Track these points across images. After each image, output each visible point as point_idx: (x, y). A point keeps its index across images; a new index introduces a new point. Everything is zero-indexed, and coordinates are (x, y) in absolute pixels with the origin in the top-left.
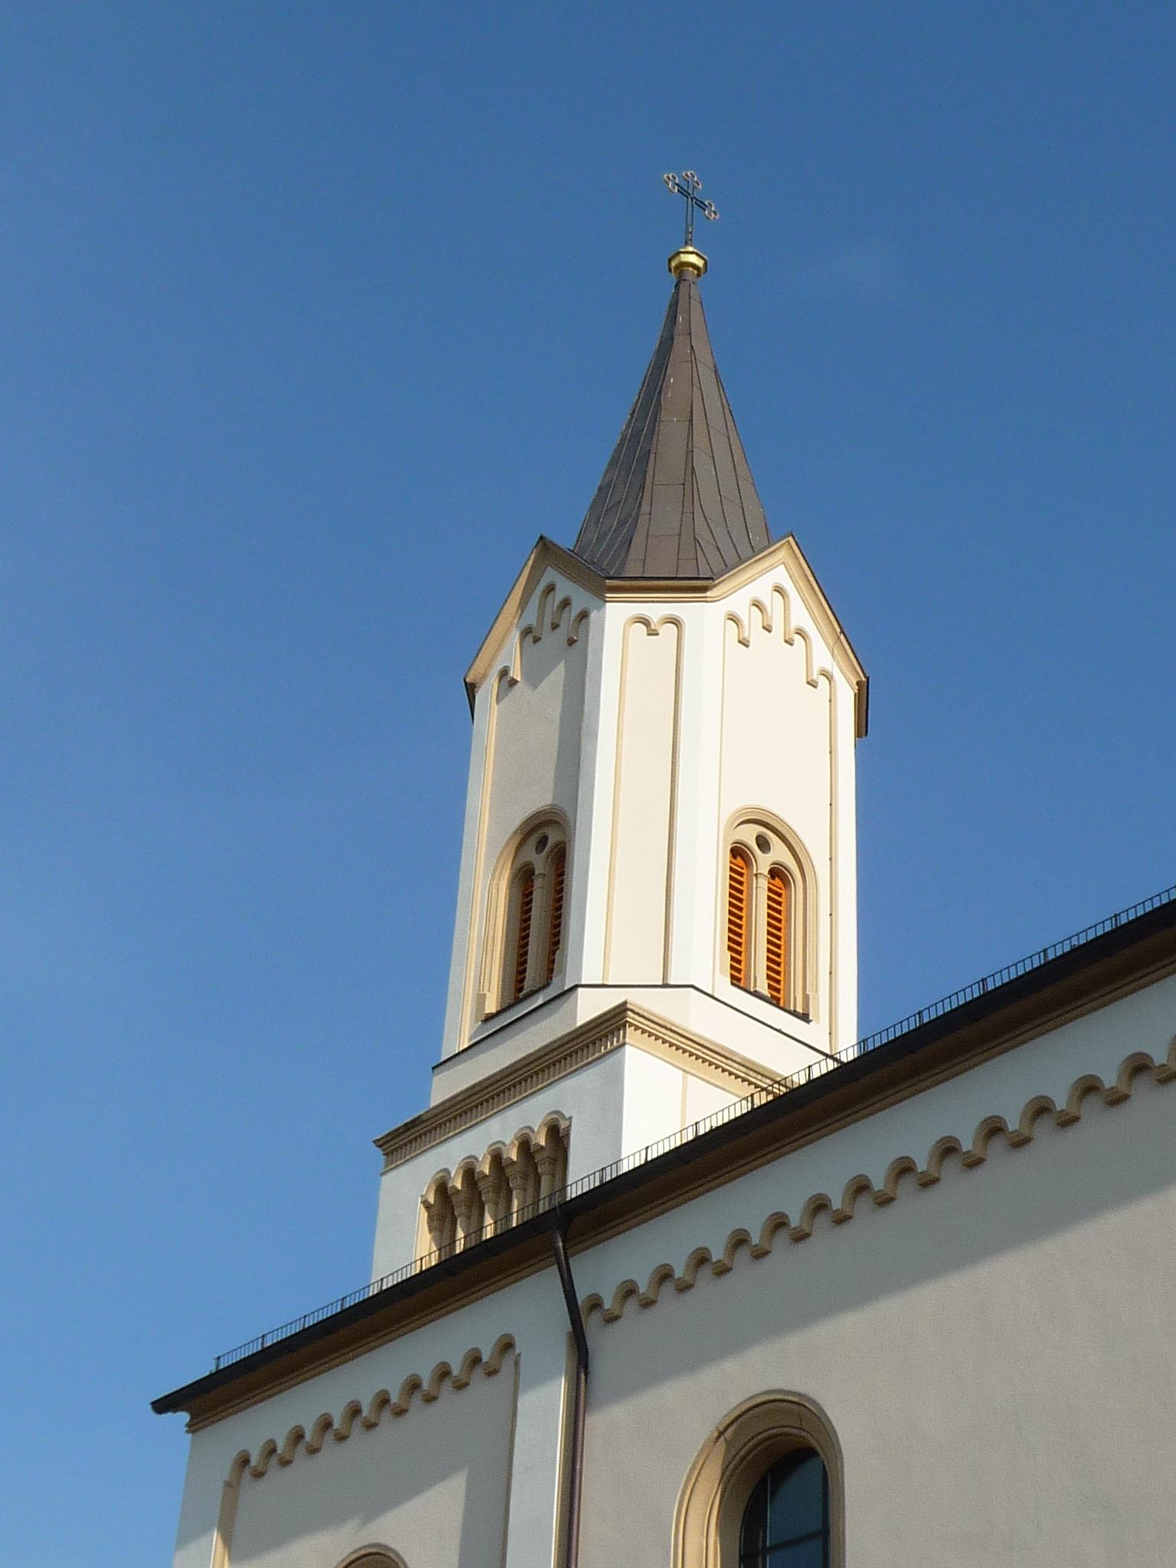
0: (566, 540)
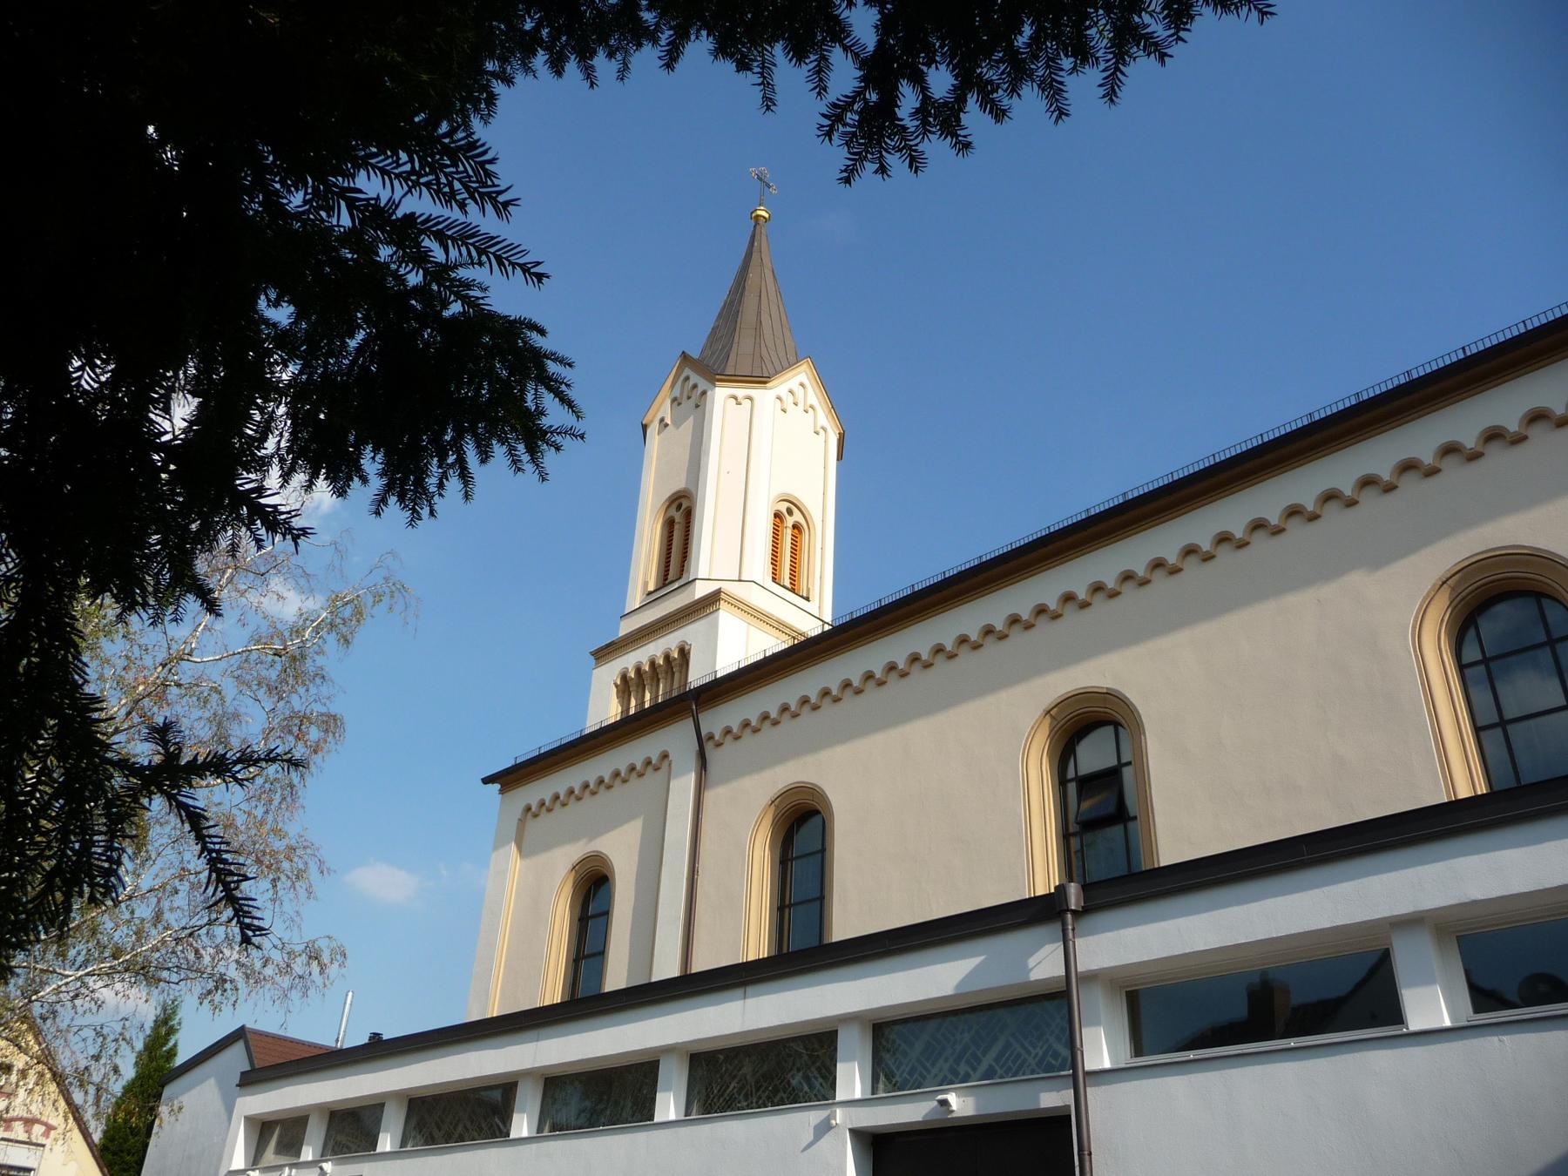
0: (695, 354)
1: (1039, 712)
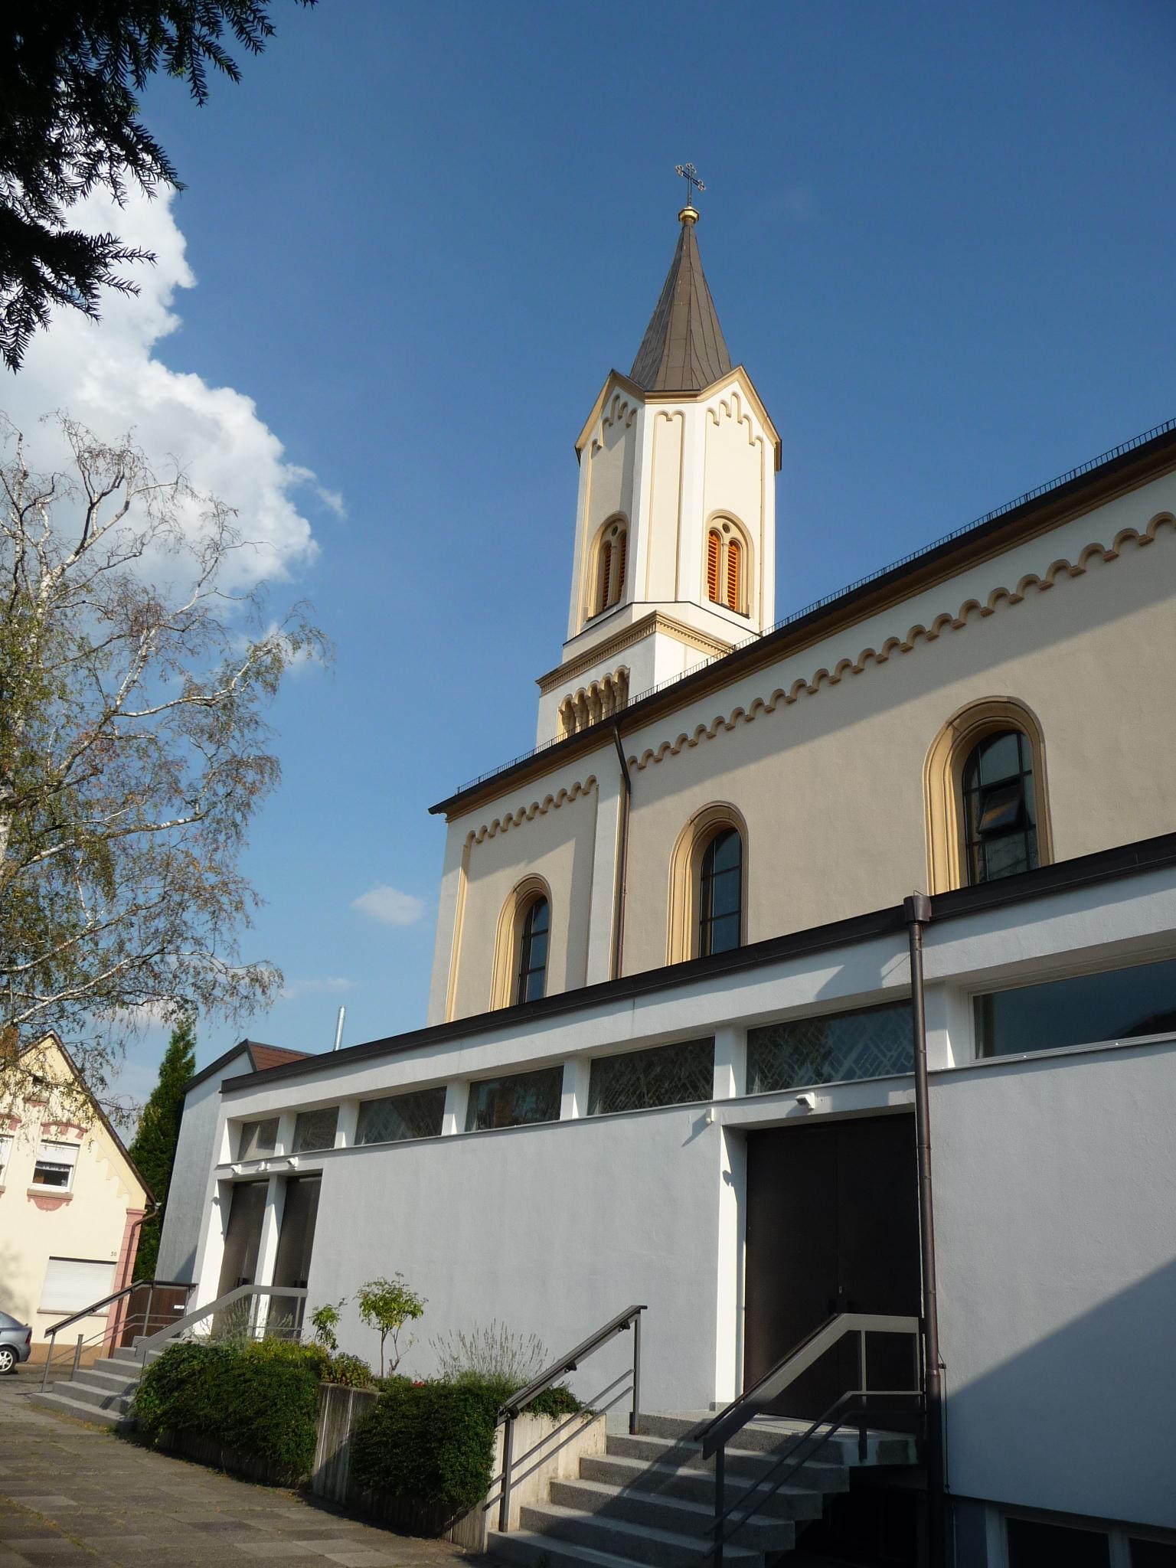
0: (625, 371)
1: (942, 723)
